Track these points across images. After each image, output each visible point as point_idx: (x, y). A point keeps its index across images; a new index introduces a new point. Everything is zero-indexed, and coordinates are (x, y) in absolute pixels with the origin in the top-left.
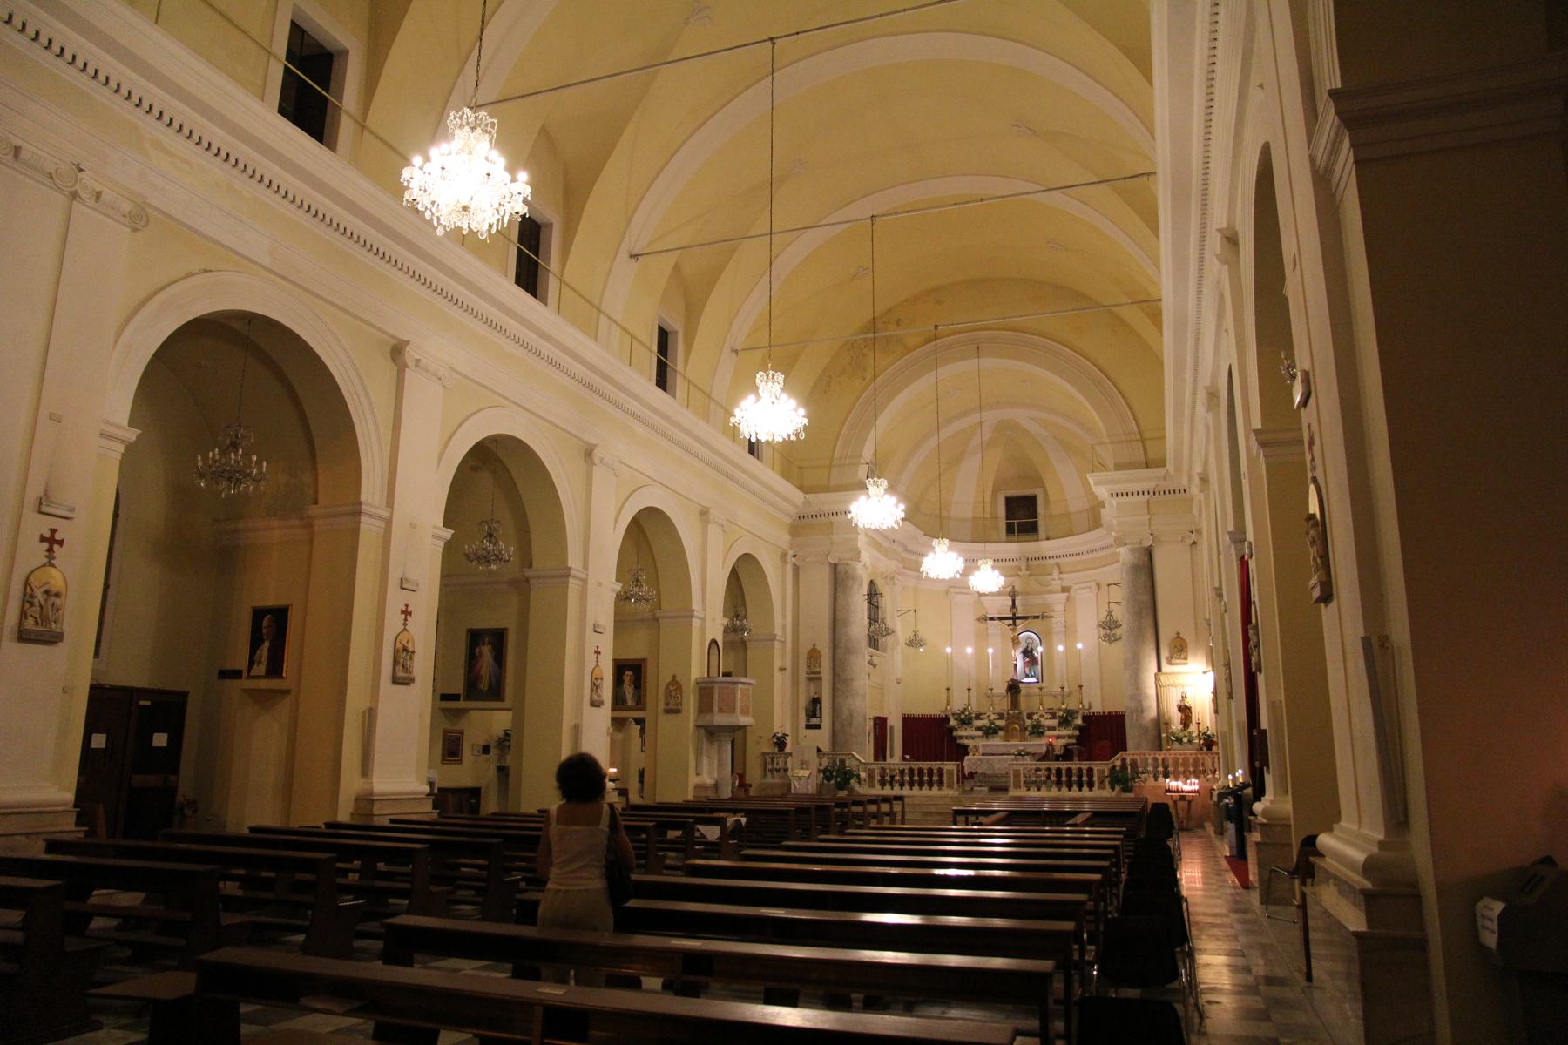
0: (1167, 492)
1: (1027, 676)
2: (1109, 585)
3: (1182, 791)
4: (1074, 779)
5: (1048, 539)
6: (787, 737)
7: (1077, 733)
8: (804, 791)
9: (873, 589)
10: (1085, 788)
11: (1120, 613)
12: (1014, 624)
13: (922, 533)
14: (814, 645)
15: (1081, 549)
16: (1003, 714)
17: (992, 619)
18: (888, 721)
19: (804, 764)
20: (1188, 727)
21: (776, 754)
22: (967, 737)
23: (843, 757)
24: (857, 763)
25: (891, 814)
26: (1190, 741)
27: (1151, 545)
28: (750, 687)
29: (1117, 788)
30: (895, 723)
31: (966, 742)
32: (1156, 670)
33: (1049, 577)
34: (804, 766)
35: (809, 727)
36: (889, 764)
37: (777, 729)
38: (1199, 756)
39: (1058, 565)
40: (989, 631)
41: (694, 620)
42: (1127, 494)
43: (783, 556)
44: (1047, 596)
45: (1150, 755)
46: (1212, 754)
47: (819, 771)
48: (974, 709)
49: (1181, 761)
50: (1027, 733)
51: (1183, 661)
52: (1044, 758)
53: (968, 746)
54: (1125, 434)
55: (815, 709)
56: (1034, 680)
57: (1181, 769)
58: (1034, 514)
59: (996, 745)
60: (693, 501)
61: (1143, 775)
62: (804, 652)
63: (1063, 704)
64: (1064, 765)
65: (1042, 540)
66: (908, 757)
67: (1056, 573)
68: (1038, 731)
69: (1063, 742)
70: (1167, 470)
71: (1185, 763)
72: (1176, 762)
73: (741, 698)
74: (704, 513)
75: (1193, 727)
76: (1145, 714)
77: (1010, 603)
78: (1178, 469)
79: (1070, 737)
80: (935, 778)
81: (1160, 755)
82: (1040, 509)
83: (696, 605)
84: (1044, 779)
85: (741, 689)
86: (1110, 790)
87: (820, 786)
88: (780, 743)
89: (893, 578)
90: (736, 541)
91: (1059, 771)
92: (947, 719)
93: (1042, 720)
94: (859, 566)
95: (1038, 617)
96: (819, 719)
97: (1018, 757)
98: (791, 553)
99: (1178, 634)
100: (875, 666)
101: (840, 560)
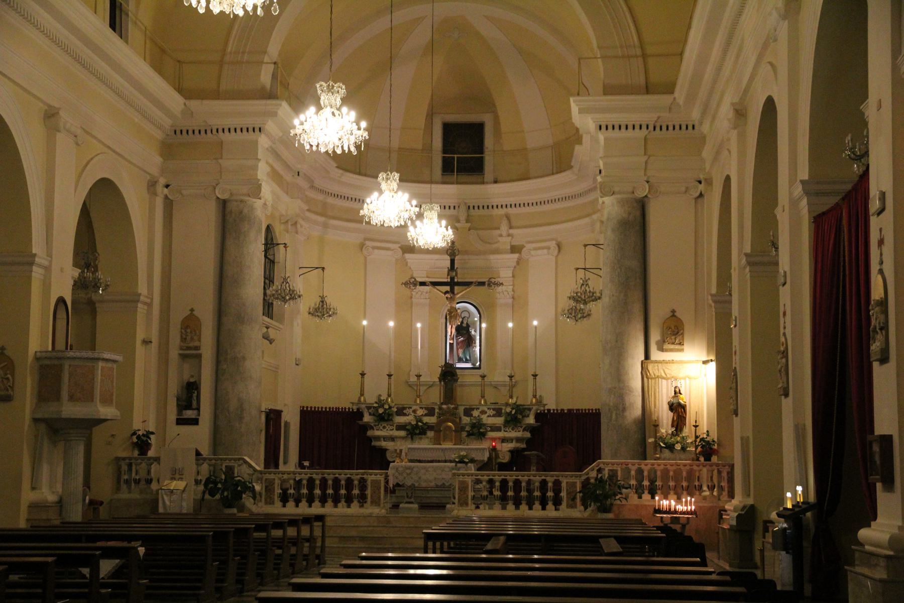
0: (671, 128)
1: (460, 360)
2: (585, 246)
3: (676, 512)
4: (523, 493)
5: (496, 182)
6: (152, 437)
7: (528, 435)
8: (176, 510)
9: (269, 238)
10: (550, 506)
11: (601, 283)
12: (452, 291)
13: (335, 165)
14: (192, 310)
15: (545, 196)
16: (434, 409)
17: (423, 284)
18: (283, 415)
19: (176, 474)
20: (681, 430)
21: (136, 459)
22: (385, 438)
23: (232, 464)
24: (251, 471)
25: (311, 539)
26: (683, 449)
27: (646, 196)
28: (115, 366)
29: (593, 507)
30: (291, 418)
31: (383, 444)
32: (643, 358)
33: (497, 232)
34: (177, 476)
35: (180, 422)
36: (283, 473)
37: (137, 425)
38: (695, 468)
39: (508, 217)
40: (414, 300)
41: (35, 268)
42: (620, 127)
43: (152, 185)
44: (492, 257)
45: (633, 465)
46: (711, 465)
47: (197, 482)
48: (393, 402)
49: (671, 473)
50: (464, 434)
51: (677, 347)
52: (484, 466)
53: (386, 450)
54: (621, 47)
55: (191, 397)
56: (469, 365)
57: (672, 484)
58: (480, 148)
59: (426, 449)
60: (38, 99)
61: (624, 491)
62: (177, 317)
63: (511, 397)
64: (511, 476)
65: (487, 183)
66: (306, 463)
67: (504, 228)
68: (478, 431)
69: (511, 446)
70: (675, 98)
71: (677, 477)
72: (666, 472)
73: (102, 381)
74: (50, 115)
75: (688, 431)
76: (627, 414)
77: (448, 264)
78: (691, 97)
79: (518, 440)
80: (356, 492)
81: (647, 466)
82: (489, 142)
83: (37, 247)
84: (485, 493)
85: (103, 368)
86: (582, 508)
87: (200, 504)
88: (142, 444)
89: (296, 223)
90: (92, 159)
91: (504, 483)
92: (359, 414)
93: (484, 417)
94: (258, 204)
95: (482, 284)
96: (195, 412)
97: (459, 465)
98: (162, 181)
99: (673, 311)
100: (271, 341)
101: (231, 194)
